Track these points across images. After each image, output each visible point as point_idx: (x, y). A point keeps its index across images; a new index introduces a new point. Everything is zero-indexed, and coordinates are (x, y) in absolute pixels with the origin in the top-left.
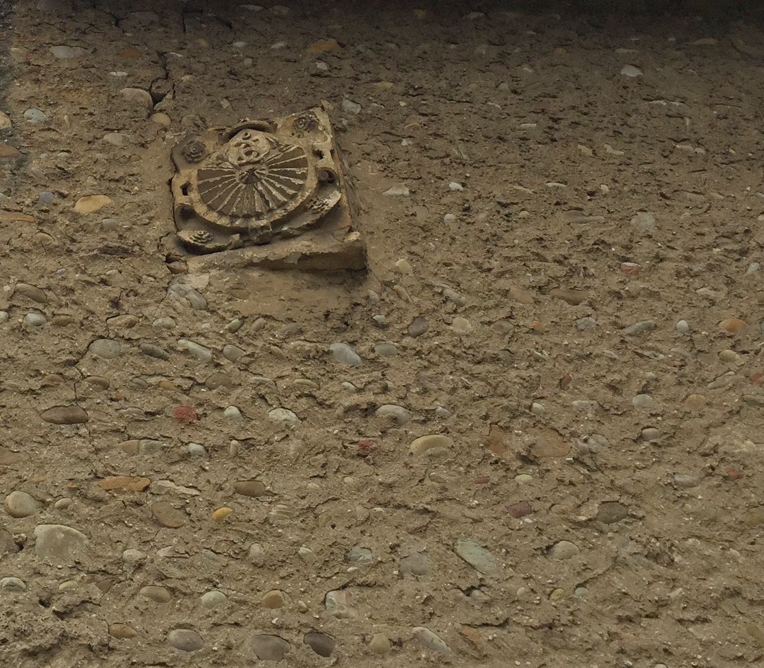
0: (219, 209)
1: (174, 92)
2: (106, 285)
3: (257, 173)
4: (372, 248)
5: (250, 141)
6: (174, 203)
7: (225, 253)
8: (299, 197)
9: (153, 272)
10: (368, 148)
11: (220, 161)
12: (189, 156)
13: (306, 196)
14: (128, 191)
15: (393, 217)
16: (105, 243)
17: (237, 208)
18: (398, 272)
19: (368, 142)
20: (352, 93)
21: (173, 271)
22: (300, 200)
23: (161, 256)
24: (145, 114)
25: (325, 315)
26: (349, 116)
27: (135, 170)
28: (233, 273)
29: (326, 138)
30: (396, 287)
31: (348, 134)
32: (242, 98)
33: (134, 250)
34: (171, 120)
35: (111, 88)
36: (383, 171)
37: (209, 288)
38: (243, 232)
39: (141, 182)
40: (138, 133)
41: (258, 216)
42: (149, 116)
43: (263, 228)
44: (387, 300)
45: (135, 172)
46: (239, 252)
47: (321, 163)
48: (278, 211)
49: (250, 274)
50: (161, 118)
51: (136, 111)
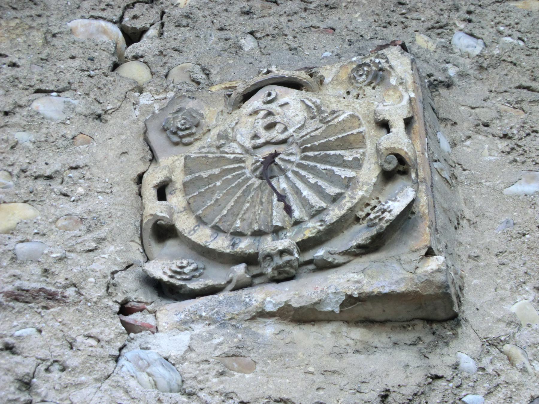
0: (213, 223)
1: (163, 25)
2: (14, 353)
3: (280, 159)
4: (473, 282)
5: (273, 107)
6: (142, 215)
7: (220, 297)
8: (347, 199)
9: (94, 331)
10: (485, 115)
11: (222, 142)
12: (175, 133)
13: (358, 197)
14: (65, 195)
15: (515, 230)
16: (17, 283)
17: (242, 220)
18: (513, 322)
19: (488, 103)
20: (470, 21)
21: (129, 328)
22: (347, 204)
23: (111, 303)
24: (107, 64)
25: (532, 397)
26: (462, 60)
27: (80, 160)
28: (230, 331)
29: (401, 97)
30: (507, 348)
31: (454, 90)
32: (279, 33)
33: (66, 294)
34: (152, 74)
35: (52, 19)
36: (509, 153)
37: (188, 356)
38: (251, 260)
39: (89, 179)
40: (92, 96)
41: (277, 231)
42: (115, 66)
43: (282, 253)
44: (490, 370)
45: (81, 164)
46: (243, 294)
47: (386, 141)
48: (310, 224)
49: (260, 332)
50: (134, 71)
51: (92, 59)
